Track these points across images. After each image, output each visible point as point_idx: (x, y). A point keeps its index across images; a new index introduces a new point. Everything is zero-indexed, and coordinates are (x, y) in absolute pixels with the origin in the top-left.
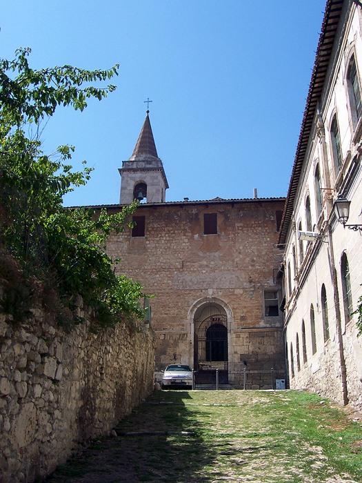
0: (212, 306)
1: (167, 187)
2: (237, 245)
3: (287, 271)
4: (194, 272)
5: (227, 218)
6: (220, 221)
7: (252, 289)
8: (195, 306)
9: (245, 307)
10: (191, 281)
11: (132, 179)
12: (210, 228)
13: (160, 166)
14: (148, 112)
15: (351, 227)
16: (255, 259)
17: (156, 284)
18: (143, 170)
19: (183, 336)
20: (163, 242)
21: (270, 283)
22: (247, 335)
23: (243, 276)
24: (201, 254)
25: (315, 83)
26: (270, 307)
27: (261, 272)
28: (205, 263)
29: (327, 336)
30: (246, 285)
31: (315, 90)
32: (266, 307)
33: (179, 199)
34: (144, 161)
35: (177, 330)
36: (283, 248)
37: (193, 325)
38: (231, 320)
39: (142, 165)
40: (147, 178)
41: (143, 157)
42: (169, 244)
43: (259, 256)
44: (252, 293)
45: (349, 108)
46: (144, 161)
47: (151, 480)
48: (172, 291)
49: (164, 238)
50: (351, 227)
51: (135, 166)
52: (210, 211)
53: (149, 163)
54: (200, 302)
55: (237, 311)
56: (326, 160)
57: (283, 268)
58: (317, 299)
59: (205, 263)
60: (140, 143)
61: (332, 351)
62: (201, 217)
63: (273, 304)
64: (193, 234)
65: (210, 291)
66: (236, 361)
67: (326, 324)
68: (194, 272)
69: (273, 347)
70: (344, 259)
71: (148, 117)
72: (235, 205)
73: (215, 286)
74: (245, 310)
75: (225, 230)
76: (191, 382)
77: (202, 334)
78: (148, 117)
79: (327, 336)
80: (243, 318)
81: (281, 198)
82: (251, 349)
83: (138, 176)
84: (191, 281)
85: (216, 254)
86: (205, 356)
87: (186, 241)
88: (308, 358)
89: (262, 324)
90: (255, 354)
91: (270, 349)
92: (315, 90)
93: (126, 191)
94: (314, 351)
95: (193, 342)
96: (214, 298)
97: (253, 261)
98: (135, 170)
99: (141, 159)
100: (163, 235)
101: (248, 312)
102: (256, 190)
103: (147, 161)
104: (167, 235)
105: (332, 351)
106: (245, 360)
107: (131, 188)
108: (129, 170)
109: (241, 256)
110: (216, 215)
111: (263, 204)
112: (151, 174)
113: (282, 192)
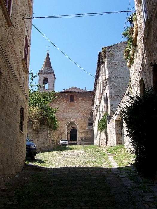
0: (72, 123)
1: (55, 79)
2: (80, 105)
4: (67, 113)
5: (77, 97)
6: (75, 97)
8: (67, 123)
9: (82, 124)
10: (66, 116)
11: (43, 76)
12: (72, 100)
13: (53, 72)
14: (48, 51)
18: (46, 73)
19: (64, 132)
21: (90, 116)
22: (83, 132)
23: (82, 115)
24: (69, 108)
26: (90, 123)
27: (87, 113)
30: (82, 117)
32: (88, 124)
33: (61, 90)
34: (47, 70)
35: (62, 130)
36: (93, 105)
37: (66, 129)
38: (78, 127)
39: (46, 71)
40: (48, 76)
41: (46, 68)
43: (86, 108)
46: (47, 70)
47: (70, 149)
51: (44, 72)
52: (71, 94)
53: (49, 71)
54: (69, 122)
57: (93, 113)
59: (70, 110)
60: (46, 63)
62: (69, 96)
63: (91, 123)
64: (66, 101)
65: (72, 119)
68: (67, 113)
71: (48, 53)
73: (73, 117)
75: (76, 100)
76: (68, 144)
77: (69, 132)
78: (48, 53)
82: (84, 136)
83: (45, 75)
84: (66, 116)
85: (73, 108)
86: (70, 139)
87: (64, 104)
89: (87, 129)
91: (90, 136)
93: (41, 81)
95: (67, 134)
96: (73, 121)
97: (85, 110)
98: (44, 73)
99: (46, 69)
102: (86, 88)
103: (48, 70)
106: (82, 139)
107: (42, 80)
108: (42, 73)
109: (81, 108)
110: (73, 95)
112: (49, 75)
113: (92, 89)
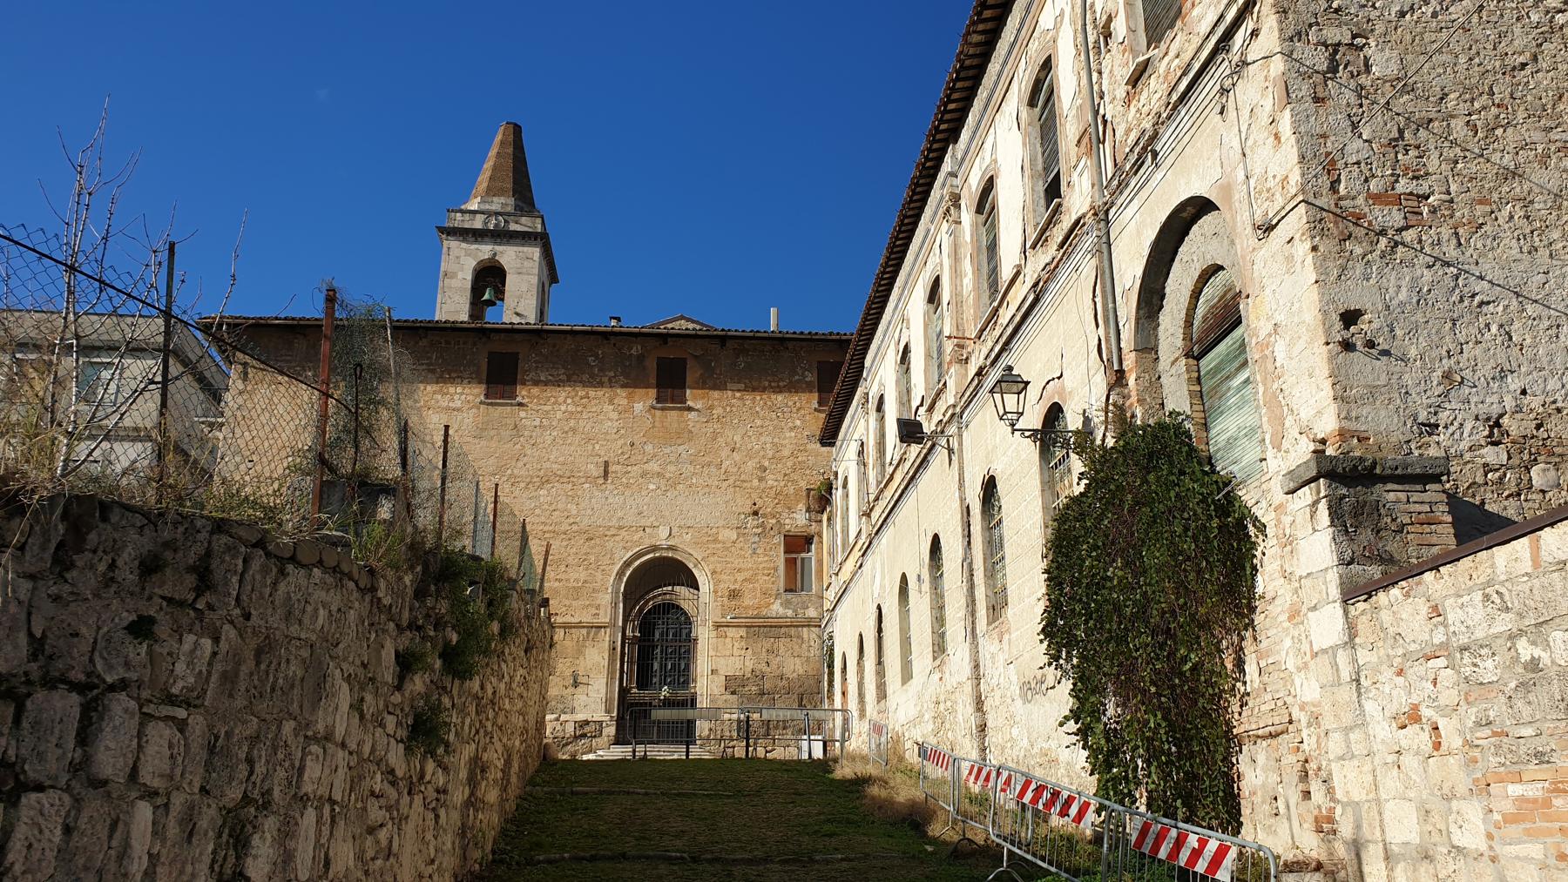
3: (838, 495)
7: (760, 530)
8: (627, 564)
15: (1027, 434)
16: (766, 464)
17: (537, 511)
20: (559, 415)
25: (950, 101)
28: (654, 466)
29: (940, 648)
31: (947, 117)
42: (572, 423)
44: (757, 539)
45: (1027, 172)
48: (575, 528)
49: (563, 408)
50: (1027, 434)
55: (724, 577)
56: (956, 273)
57: (829, 488)
58: (915, 562)
61: (950, 681)
66: (716, 692)
67: (939, 620)
69: (797, 661)
70: (990, 486)
72: (729, 344)
74: (740, 577)
79: (940, 648)
80: (734, 595)
81: (831, 334)
82: (749, 665)
87: (615, 415)
88: (889, 691)
90: (759, 677)
92: (947, 117)
94: (907, 675)
96: (671, 548)
100: (561, 400)
101: (745, 580)
104: (569, 401)
105: (950, 681)
110: (684, 361)
111: (790, 345)
113: (849, 326)
